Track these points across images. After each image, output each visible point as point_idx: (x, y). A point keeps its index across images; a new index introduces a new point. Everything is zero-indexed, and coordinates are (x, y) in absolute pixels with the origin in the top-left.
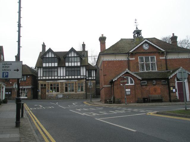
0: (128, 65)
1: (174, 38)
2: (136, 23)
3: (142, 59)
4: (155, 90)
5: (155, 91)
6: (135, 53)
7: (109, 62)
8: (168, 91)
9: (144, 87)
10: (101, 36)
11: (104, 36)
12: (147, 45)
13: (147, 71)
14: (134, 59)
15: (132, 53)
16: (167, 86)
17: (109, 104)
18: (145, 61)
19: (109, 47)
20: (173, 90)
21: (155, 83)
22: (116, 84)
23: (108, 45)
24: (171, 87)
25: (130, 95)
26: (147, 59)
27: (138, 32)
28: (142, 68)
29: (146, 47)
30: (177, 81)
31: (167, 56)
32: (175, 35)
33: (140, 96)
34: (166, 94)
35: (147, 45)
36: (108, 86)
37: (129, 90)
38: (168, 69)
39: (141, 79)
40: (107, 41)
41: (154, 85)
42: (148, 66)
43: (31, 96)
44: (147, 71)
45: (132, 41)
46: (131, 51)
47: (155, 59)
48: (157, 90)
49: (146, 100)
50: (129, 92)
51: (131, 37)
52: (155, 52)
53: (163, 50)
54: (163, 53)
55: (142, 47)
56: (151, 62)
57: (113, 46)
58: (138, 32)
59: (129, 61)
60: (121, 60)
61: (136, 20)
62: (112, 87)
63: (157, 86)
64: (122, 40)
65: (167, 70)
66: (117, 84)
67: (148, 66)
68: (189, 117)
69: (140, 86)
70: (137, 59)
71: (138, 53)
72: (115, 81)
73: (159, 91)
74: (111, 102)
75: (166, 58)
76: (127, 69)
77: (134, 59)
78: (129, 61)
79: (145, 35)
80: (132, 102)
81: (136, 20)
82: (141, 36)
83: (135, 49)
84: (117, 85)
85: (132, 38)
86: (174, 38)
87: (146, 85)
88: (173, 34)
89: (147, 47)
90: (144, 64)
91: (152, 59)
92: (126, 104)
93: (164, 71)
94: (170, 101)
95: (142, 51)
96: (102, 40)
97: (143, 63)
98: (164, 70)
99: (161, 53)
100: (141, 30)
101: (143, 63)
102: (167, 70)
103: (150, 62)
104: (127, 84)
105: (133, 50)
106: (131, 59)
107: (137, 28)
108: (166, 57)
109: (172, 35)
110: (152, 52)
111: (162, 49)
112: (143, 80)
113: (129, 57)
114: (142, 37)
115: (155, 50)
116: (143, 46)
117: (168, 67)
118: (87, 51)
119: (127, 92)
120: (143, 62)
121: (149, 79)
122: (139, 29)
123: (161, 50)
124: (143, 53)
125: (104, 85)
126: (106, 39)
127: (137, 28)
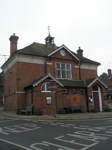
0: (45, 70)
1: (81, 51)
2: (49, 29)
3: (58, 65)
4: (75, 99)
5: (75, 100)
6: (53, 58)
7: (24, 64)
8: (86, 100)
9: (65, 95)
10: (13, 35)
11: (16, 35)
12: (64, 52)
13: (63, 79)
14: (51, 64)
15: (50, 58)
16: (85, 96)
17: (27, 115)
18: (62, 68)
19: (20, 49)
20: (90, 100)
21: (66, 92)
22: (36, 90)
23: (21, 45)
24: (89, 96)
25: (50, 104)
26: (63, 67)
27: (50, 39)
28: (58, 75)
29: (63, 53)
30: (98, 92)
31: (80, 66)
32: (81, 49)
33: (61, 106)
34: (85, 104)
35: (64, 51)
36: (21, 92)
37: (50, 98)
38: (81, 78)
39: (63, 86)
40: (18, 41)
41: (74, 94)
42: (64, 73)
43: (51, 115)
44: (63, 79)
45: (45, 46)
46: (49, 55)
47: (71, 67)
48: (76, 99)
49: (68, 110)
50: (50, 101)
51: (44, 43)
52: (71, 60)
53: (78, 59)
54: (78, 61)
55: (60, 52)
56: (67, 69)
57: (27, 47)
58: (50, 39)
59: (46, 65)
60: (38, 64)
61: (49, 27)
62: (26, 93)
63: (76, 95)
64: (34, 43)
65: (80, 79)
66: (37, 91)
67: (64, 73)
68: (111, 131)
69: (62, 94)
70: (54, 65)
71: (55, 58)
72: (36, 86)
73: (78, 100)
74: (30, 112)
75: (79, 67)
76: (49, 74)
77: (51, 64)
78: (46, 65)
79: (58, 43)
80: (53, 112)
81: (49, 27)
82: (54, 43)
83: (53, 53)
84: (38, 91)
85: (45, 43)
86: (81, 51)
87: (67, 94)
88: (80, 47)
89: (64, 54)
90: (60, 70)
91: (68, 66)
92: (55, 117)
93: (78, 80)
94: (88, 111)
95: (59, 57)
96: (14, 39)
97: (59, 69)
98: (77, 79)
99: (76, 61)
100: (54, 38)
101: (59, 69)
102: (80, 79)
103: (66, 70)
104: (42, 92)
105: (51, 54)
106: (48, 64)
107: (49, 35)
108: (79, 66)
109: (78, 49)
110: (68, 60)
111: (77, 58)
112: (65, 87)
113: (46, 62)
114: (54, 45)
115: (71, 58)
116: (60, 52)
117: (81, 76)
118: (34, 42)
119: (48, 101)
120: (59, 68)
121: (69, 87)
122: (52, 36)
123: (76, 59)
124: (60, 59)
125: (17, 91)
126: (18, 39)
127: (49, 35)
